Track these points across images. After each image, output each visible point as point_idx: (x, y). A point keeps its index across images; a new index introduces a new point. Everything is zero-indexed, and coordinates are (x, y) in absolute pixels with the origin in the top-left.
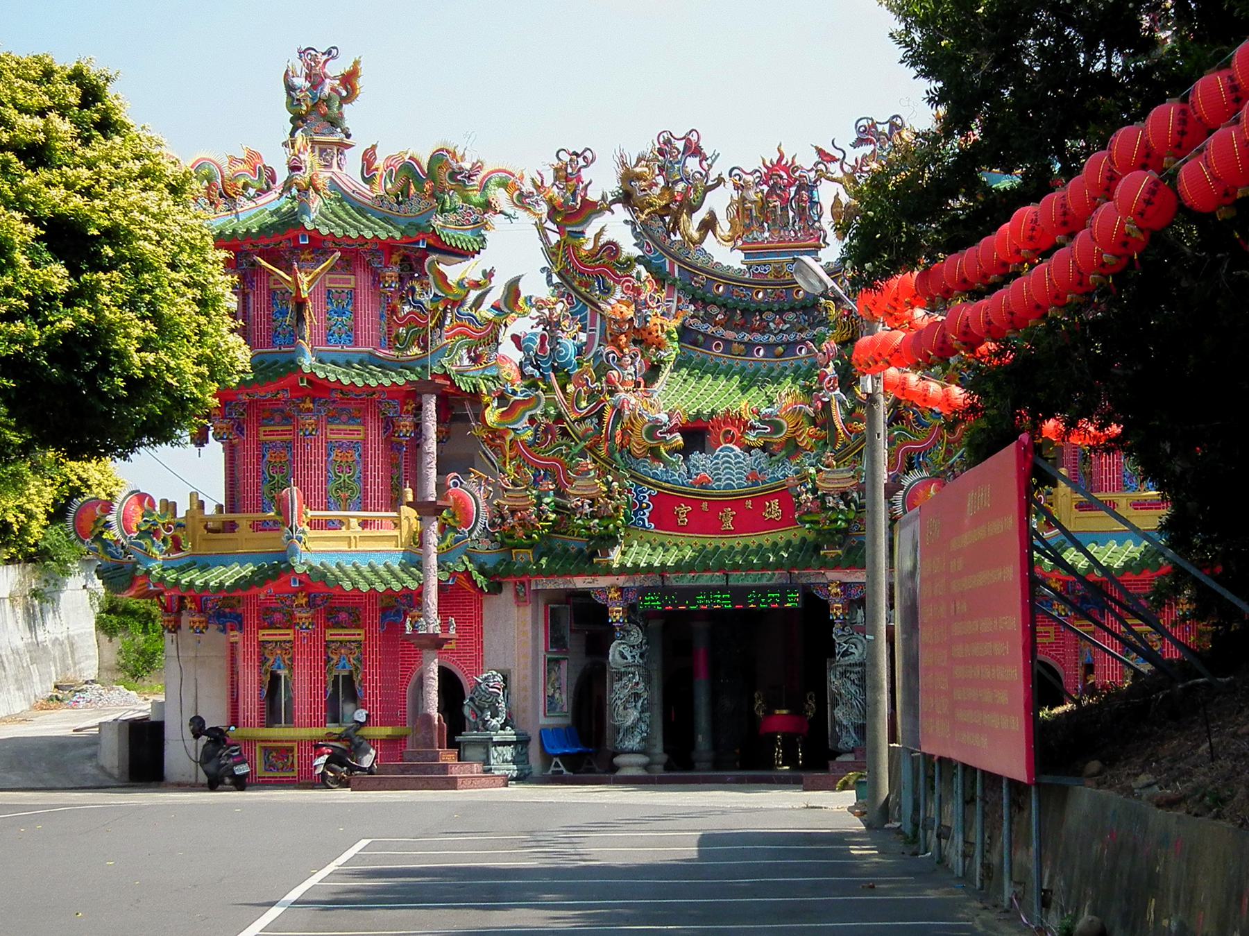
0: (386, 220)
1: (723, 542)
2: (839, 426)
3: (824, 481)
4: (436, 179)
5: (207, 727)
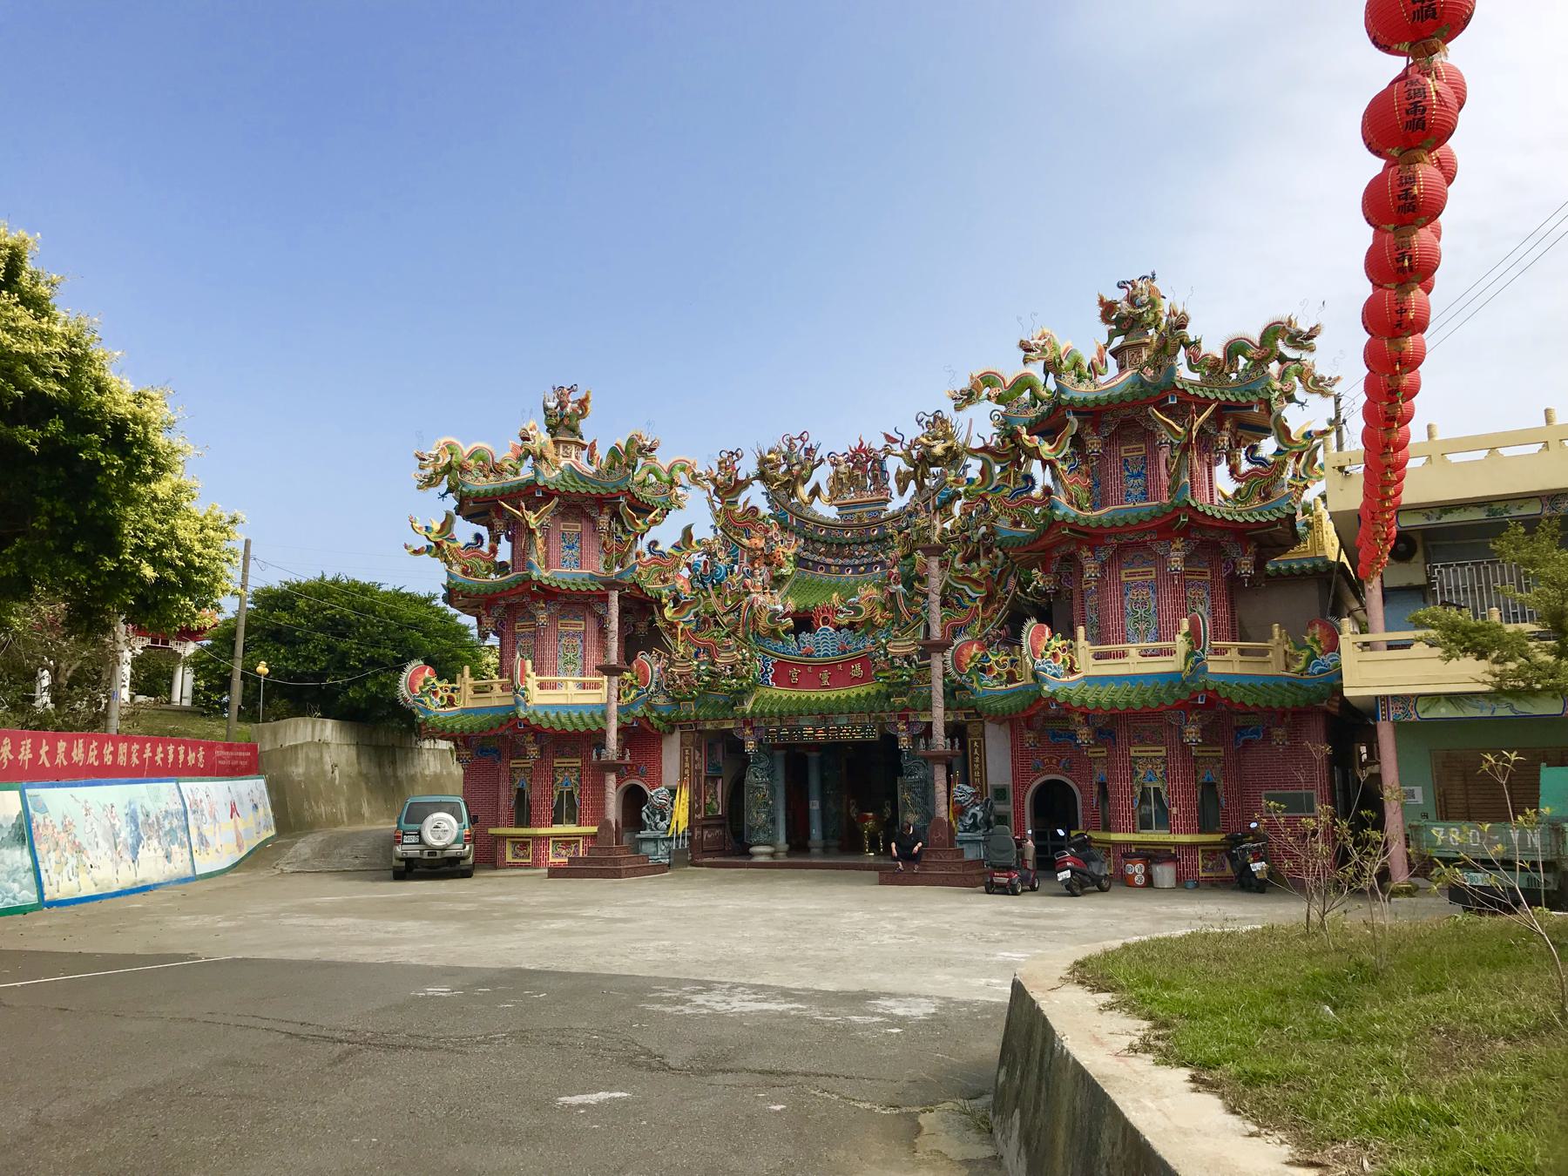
4: (638, 449)
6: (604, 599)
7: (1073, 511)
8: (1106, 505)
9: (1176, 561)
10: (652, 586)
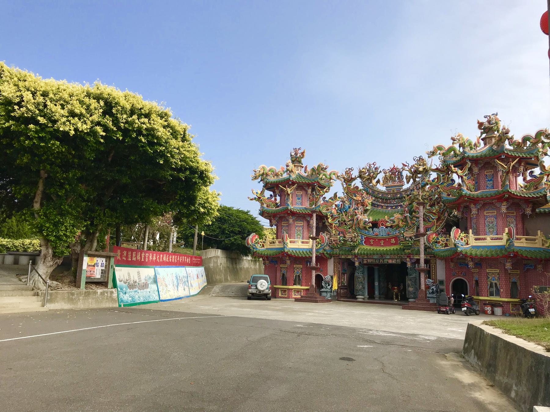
4: (321, 169)
6: (311, 216)
7: (469, 192)
8: (479, 190)
9: (504, 209)
10: (324, 211)
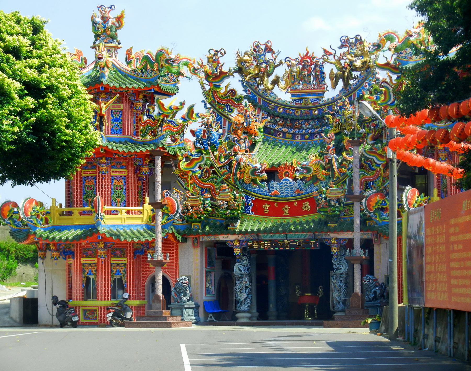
0: (137, 80)
1: (285, 220)
2: (336, 170)
3: (330, 193)
5: (59, 300)
